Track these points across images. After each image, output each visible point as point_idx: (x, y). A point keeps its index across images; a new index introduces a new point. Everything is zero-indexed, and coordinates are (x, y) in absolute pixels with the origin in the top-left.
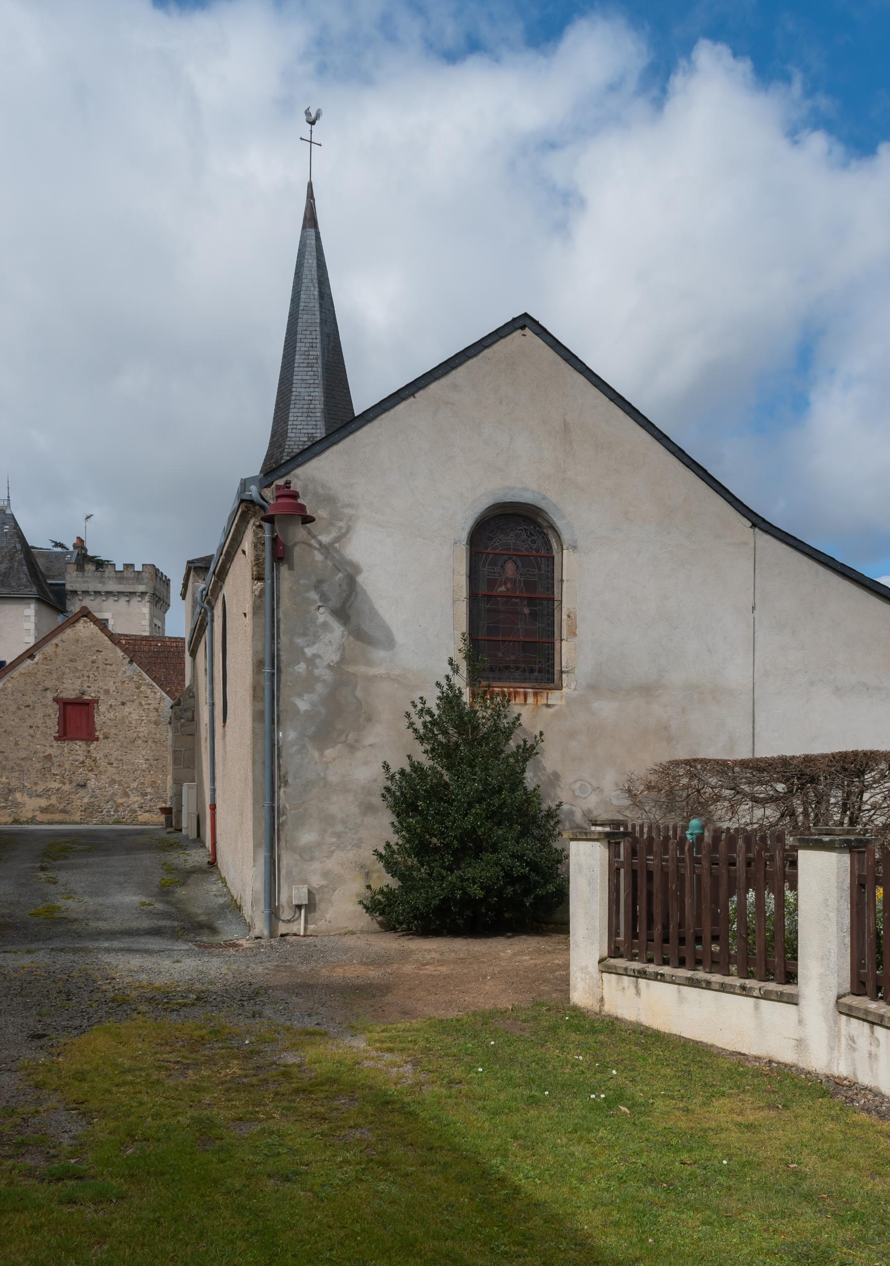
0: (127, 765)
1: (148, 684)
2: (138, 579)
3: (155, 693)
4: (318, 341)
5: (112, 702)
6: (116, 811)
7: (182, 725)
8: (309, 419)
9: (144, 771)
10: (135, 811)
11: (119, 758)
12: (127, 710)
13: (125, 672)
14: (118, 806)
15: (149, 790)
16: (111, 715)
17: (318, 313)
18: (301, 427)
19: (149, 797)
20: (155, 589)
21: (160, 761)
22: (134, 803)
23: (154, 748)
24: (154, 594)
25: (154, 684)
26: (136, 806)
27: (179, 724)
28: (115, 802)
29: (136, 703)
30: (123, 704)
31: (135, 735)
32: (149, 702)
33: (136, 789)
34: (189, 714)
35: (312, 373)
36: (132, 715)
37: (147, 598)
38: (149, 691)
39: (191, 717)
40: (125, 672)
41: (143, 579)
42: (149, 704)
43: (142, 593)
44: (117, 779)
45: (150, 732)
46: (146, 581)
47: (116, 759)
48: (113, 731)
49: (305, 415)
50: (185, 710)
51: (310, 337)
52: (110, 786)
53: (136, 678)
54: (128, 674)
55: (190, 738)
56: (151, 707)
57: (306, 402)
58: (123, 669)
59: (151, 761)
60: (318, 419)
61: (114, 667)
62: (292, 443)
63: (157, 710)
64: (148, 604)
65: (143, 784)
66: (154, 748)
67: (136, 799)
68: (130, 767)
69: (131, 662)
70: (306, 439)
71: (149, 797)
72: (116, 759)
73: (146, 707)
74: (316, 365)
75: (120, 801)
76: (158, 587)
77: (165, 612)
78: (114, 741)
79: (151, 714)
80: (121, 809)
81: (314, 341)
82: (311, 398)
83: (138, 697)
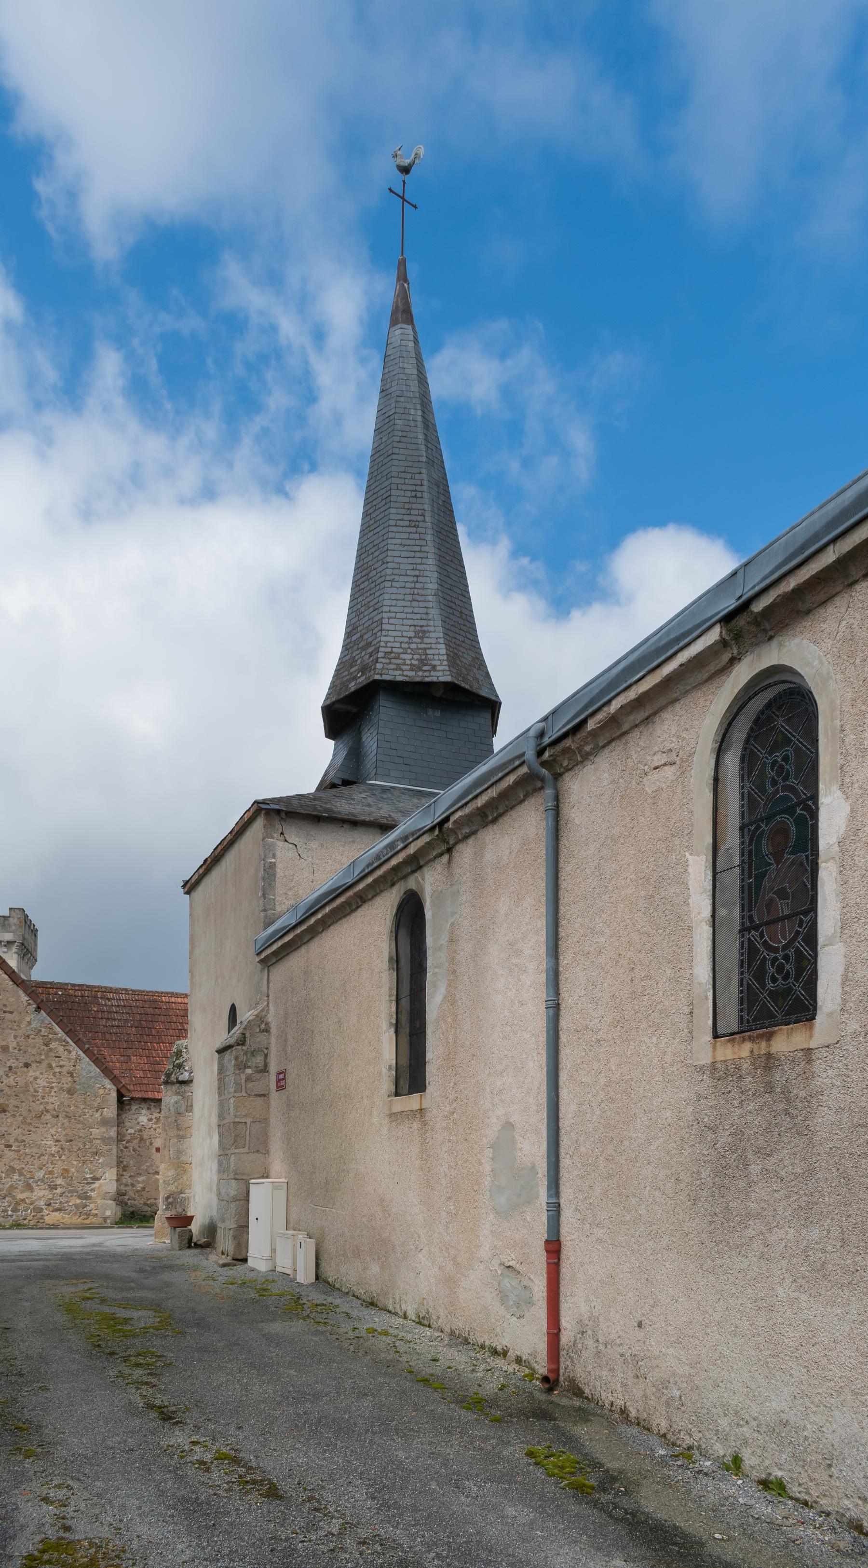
0: (30, 1147)
1: (60, 1040)
2: (4, 925)
3: (70, 1052)
4: (425, 488)
5: (11, 1062)
6: (15, 1210)
7: (248, 1079)
8: (415, 604)
9: (53, 1155)
10: (41, 1210)
11: (20, 1139)
12: (31, 1073)
13: (29, 1023)
14: (17, 1204)
15: (59, 1181)
16: (11, 1081)
17: (423, 447)
18: (404, 616)
19: (59, 1191)
20: (24, 939)
21: (74, 1143)
22: (40, 1198)
23: (67, 1124)
24: (23, 944)
25: (68, 1039)
26: (42, 1203)
27: (243, 1077)
28: (14, 1198)
29: (45, 1064)
30: (27, 1065)
31: (42, 1107)
32: (62, 1063)
33: (42, 1180)
34: (259, 1060)
35: (417, 536)
36: (39, 1081)
37: (14, 948)
38: (61, 1049)
39: (261, 1065)
40: (29, 1023)
41: (9, 925)
42: (61, 1066)
43: (9, 942)
44: (17, 1167)
45: (62, 1103)
46: (13, 928)
47: (16, 1140)
48: (13, 1102)
49: (409, 598)
50: (253, 1053)
51: (411, 482)
52: (8, 1176)
53: (44, 1032)
54: (33, 1026)
55: (260, 1100)
56: (64, 1070)
57: (410, 579)
58: (28, 1019)
59: (63, 1142)
60: (430, 605)
61: (15, 1016)
62: (392, 639)
63: (71, 1074)
64: (15, 956)
65: (51, 1173)
66: (67, 1124)
67: (41, 1193)
68: (34, 1150)
69: (38, 1009)
70: (412, 634)
71: (59, 1191)
72: (16, 1140)
73: (57, 1070)
74: (421, 524)
75: (20, 1196)
76: (27, 936)
77: (31, 968)
78: (14, 1116)
79: (64, 1080)
80: (21, 1207)
81: (418, 488)
82: (417, 573)
83: (47, 1056)
